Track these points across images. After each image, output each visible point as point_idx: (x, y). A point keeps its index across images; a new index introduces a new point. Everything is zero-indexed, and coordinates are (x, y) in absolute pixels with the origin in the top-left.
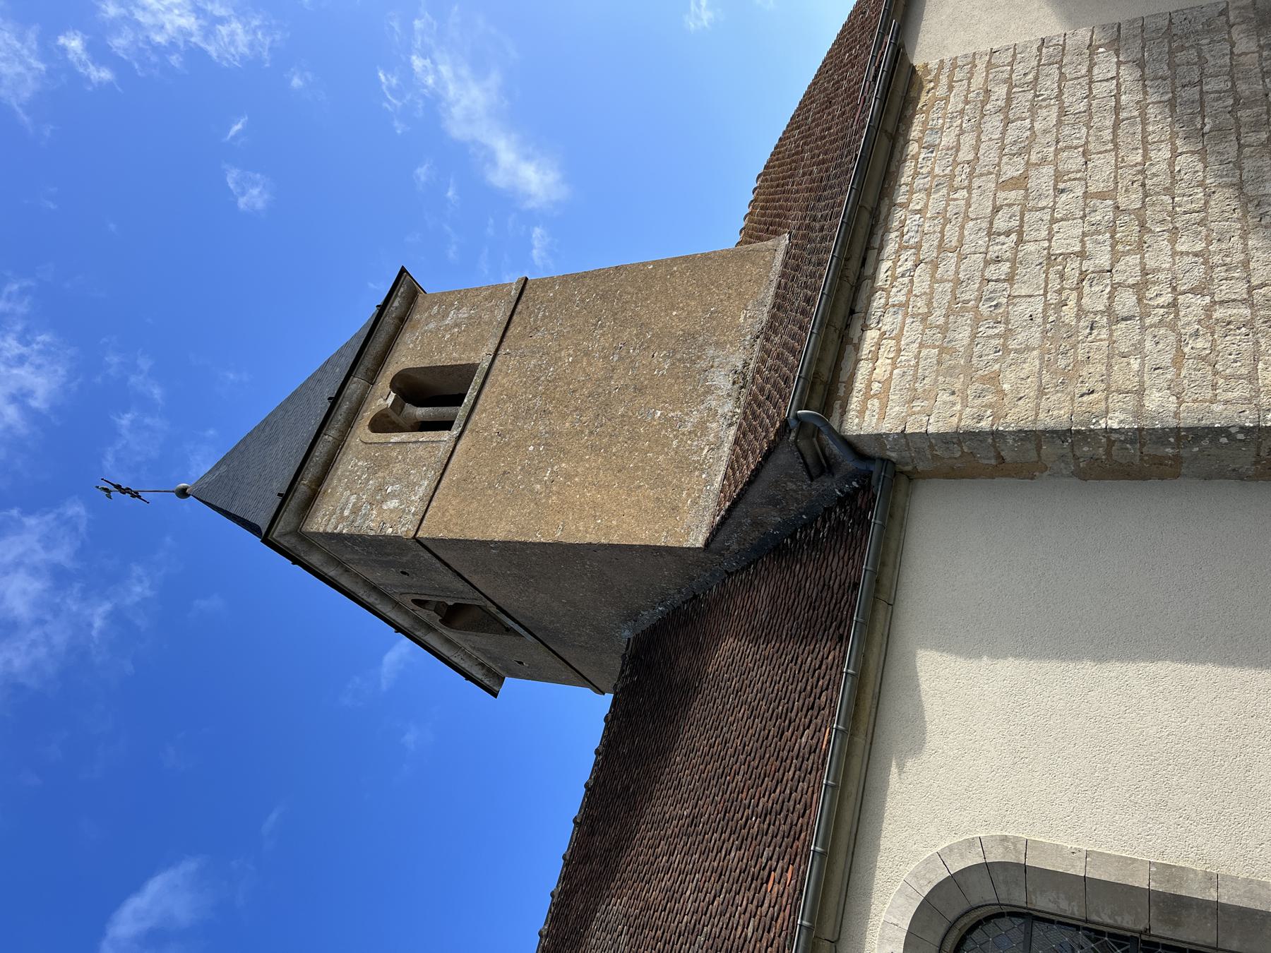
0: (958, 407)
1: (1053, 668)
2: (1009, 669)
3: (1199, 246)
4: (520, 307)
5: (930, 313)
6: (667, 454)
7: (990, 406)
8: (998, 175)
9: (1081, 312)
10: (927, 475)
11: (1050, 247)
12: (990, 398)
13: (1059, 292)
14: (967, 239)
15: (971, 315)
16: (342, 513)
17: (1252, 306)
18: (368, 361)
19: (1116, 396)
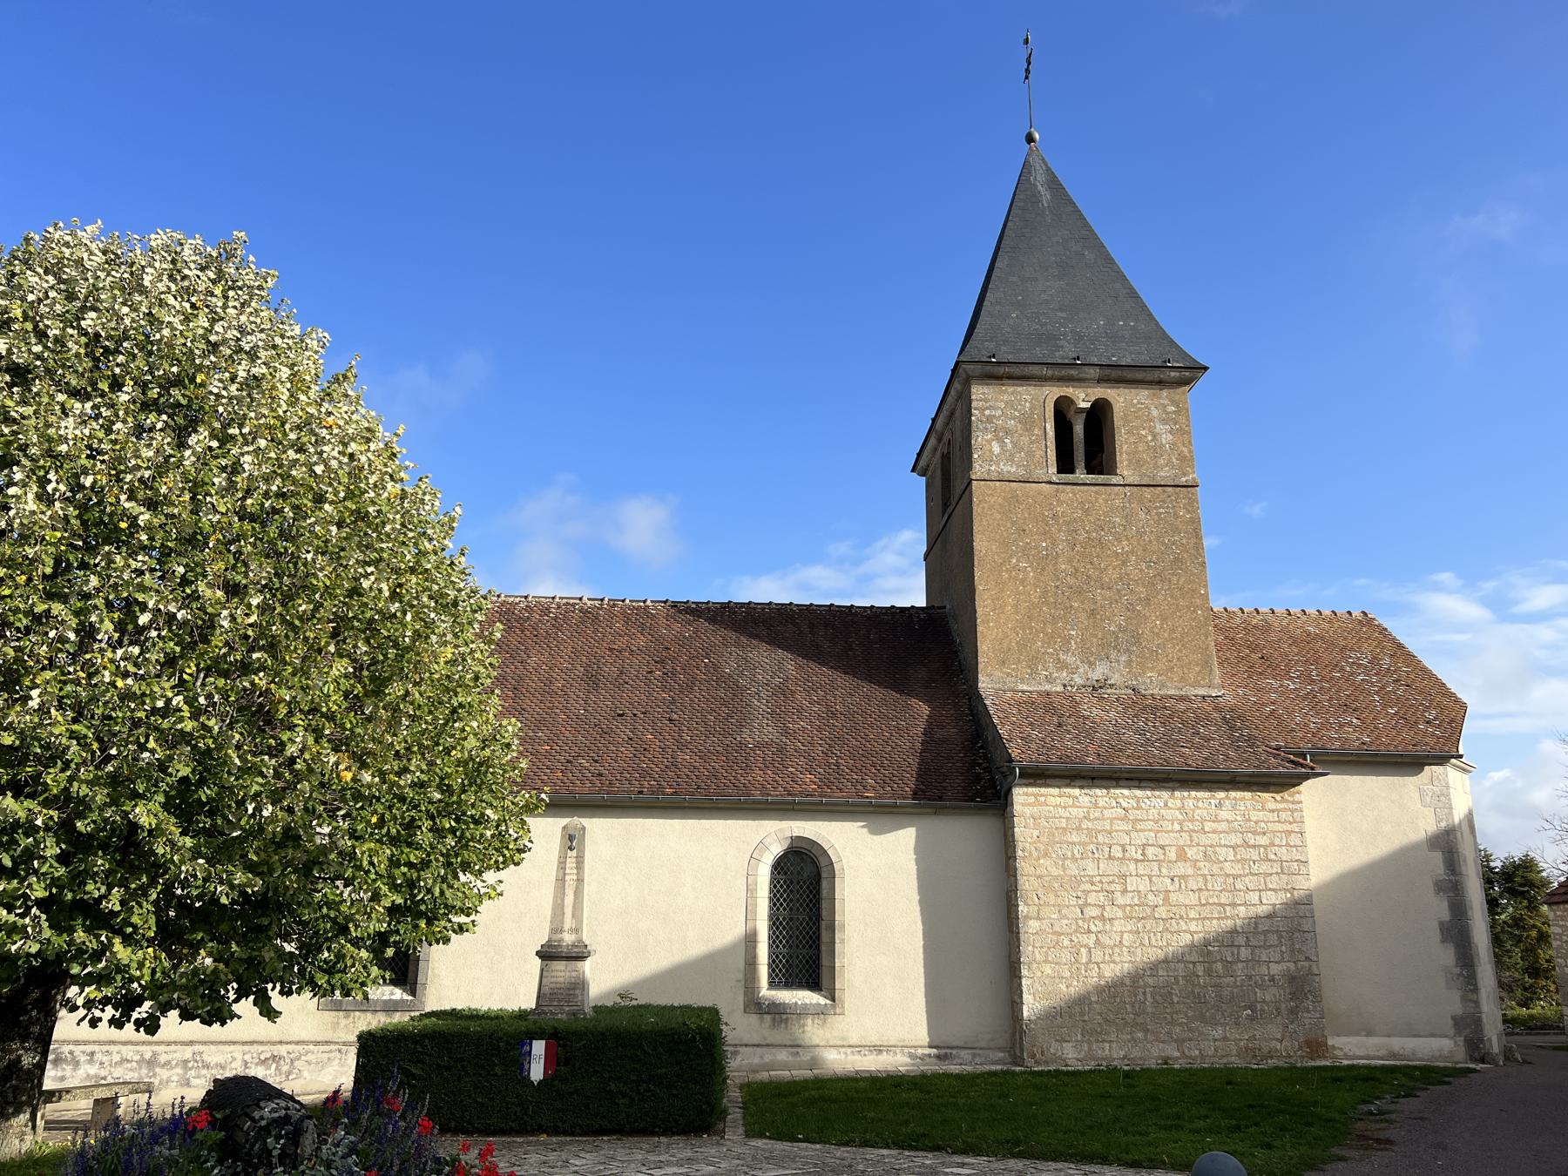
0: (1029, 840)
1: (915, 884)
2: (912, 868)
3: (1125, 943)
4: (1170, 489)
5: (1089, 820)
6: (1043, 647)
7: (1030, 854)
8: (1189, 846)
9: (1086, 892)
10: (1004, 823)
11: (1131, 875)
12: (1035, 854)
13: (1101, 882)
14: (1141, 834)
15: (1087, 840)
16: (987, 408)
17: (1087, 963)
18: (1115, 373)
19: (1036, 908)
